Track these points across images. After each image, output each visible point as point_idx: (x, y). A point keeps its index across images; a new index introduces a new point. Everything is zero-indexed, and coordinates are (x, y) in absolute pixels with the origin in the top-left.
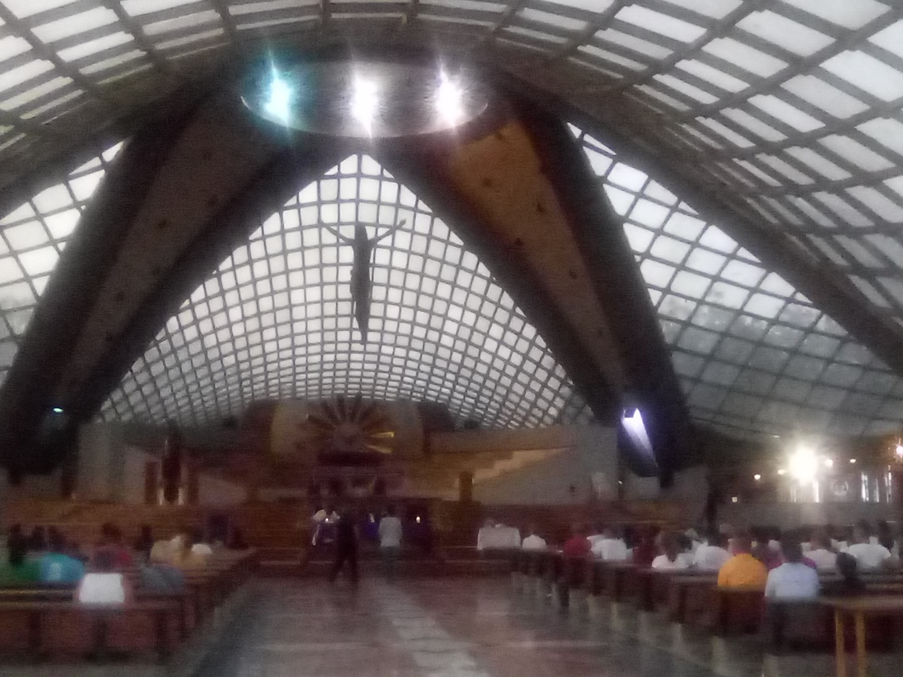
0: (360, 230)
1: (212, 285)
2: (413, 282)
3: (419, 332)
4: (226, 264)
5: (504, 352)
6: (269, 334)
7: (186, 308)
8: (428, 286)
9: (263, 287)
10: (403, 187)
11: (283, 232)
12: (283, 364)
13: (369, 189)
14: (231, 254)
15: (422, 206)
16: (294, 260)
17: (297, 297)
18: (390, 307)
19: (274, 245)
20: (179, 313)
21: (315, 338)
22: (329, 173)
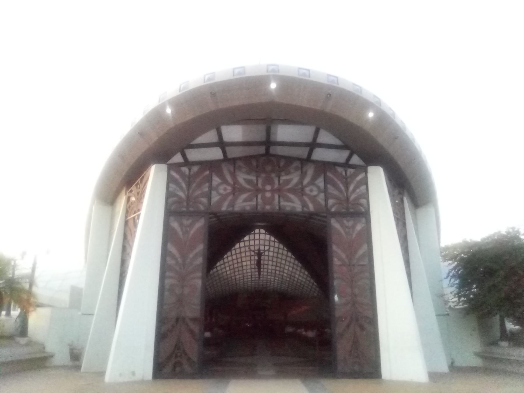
0: (259, 250)
1: (222, 262)
2: (275, 259)
4: (225, 256)
6: (237, 273)
7: (252, 234)
8: (279, 260)
9: (235, 261)
13: (262, 236)
14: (235, 246)
15: (276, 240)
17: (244, 264)
19: (238, 251)
20: (250, 234)
21: (249, 274)
22: (241, 241)
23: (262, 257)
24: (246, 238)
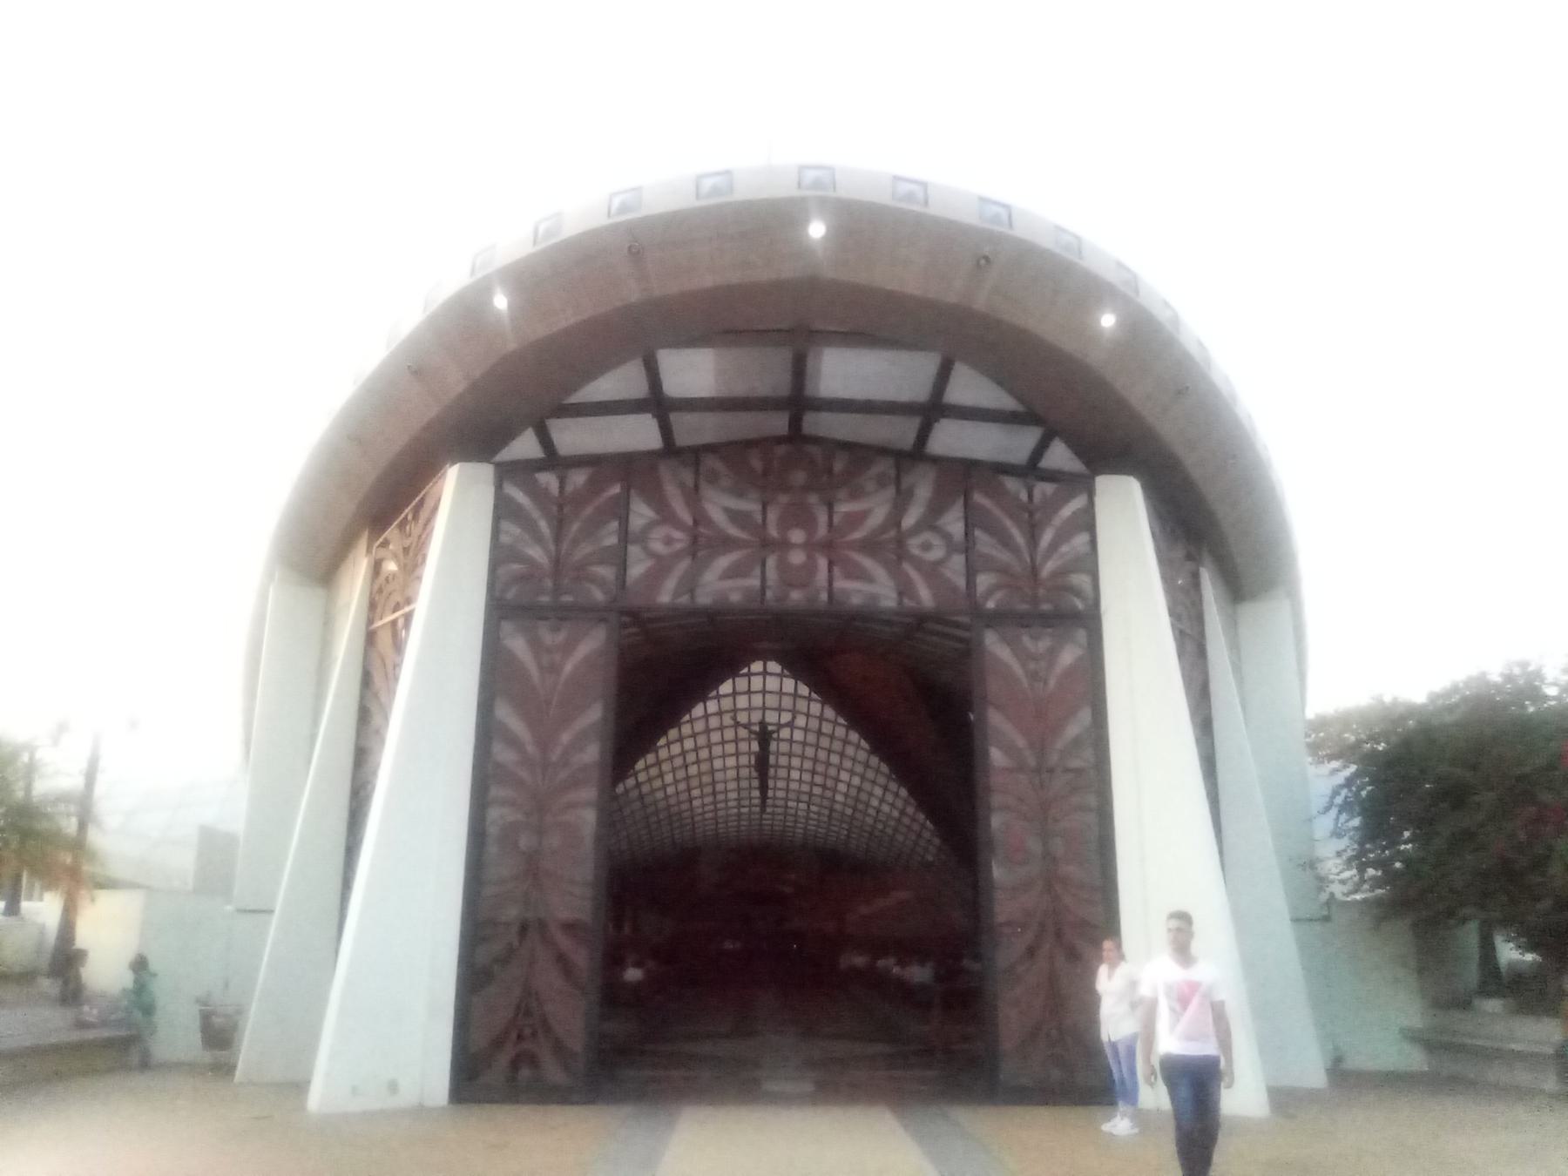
0: (763, 724)
1: (651, 758)
3: (817, 791)
4: (662, 742)
5: (886, 808)
9: (691, 757)
10: (798, 682)
11: (706, 716)
12: (707, 816)
13: (773, 684)
16: (715, 737)
18: (733, 745)
19: (700, 726)
21: (733, 795)
23: (773, 746)
24: (726, 688)
